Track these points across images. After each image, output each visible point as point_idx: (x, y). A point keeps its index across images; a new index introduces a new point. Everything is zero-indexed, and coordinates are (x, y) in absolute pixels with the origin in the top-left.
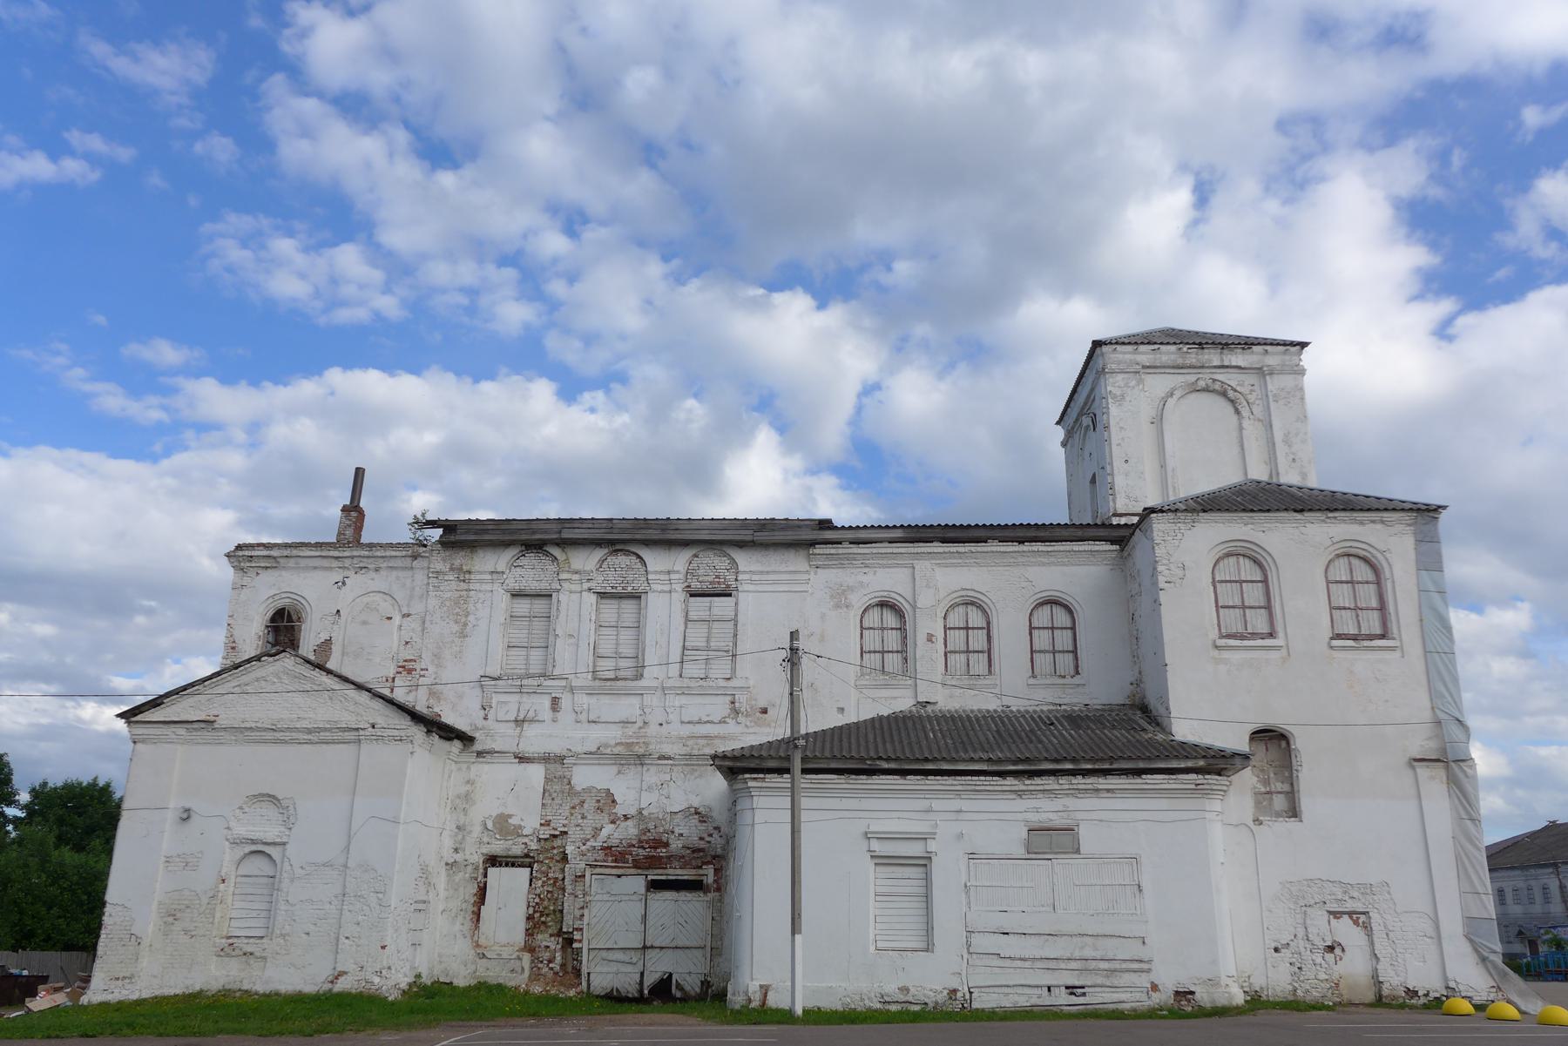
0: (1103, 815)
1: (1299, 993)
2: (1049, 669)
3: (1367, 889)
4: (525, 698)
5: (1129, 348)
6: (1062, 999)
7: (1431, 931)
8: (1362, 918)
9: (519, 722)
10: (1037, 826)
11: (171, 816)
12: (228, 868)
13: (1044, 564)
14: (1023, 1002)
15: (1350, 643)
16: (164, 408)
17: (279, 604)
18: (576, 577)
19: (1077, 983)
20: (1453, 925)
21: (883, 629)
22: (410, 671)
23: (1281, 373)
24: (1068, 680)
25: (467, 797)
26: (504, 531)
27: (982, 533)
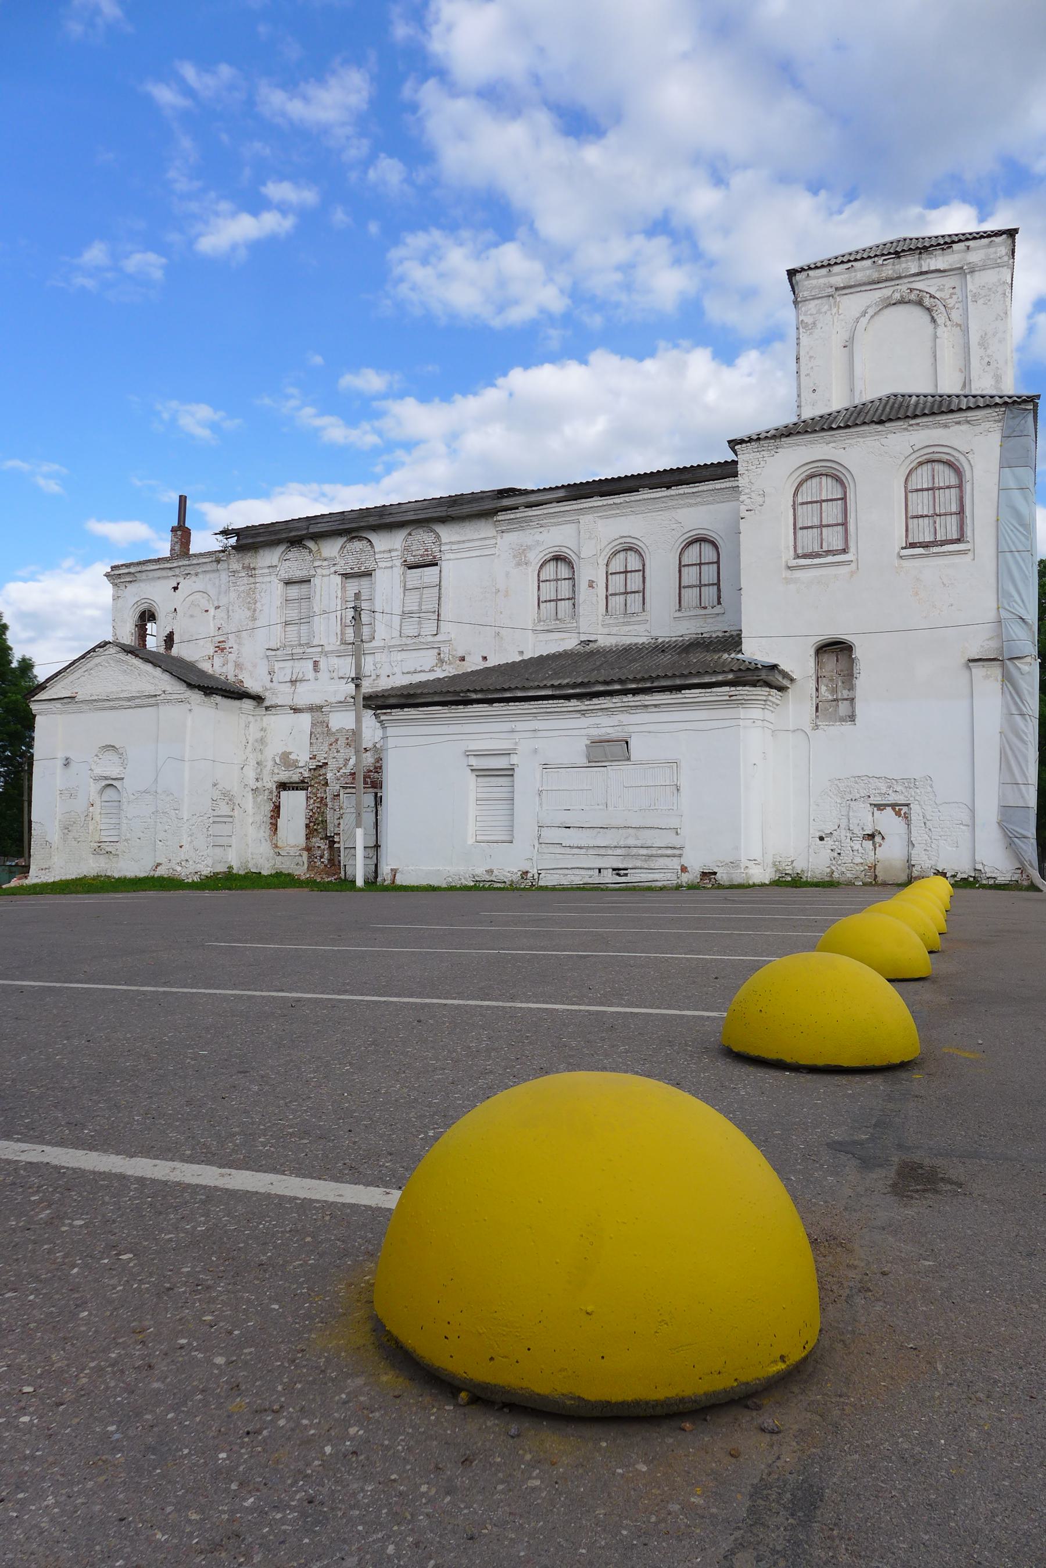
0: (651, 727)
1: (836, 875)
2: (695, 602)
3: (911, 783)
4: (297, 664)
5: (824, 271)
6: (609, 877)
7: (967, 819)
8: (905, 809)
9: (293, 682)
10: (597, 739)
11: (60, 763)
12: (94, 796)
13: (691, 505)
14: (577, 880)
15: (921, 551)
16: (380, 433)
17: (142, 608)
18: (325, 563)
19: (621, 866)
20: (988, 812)
21: (557, 580)
22: (222, 650)
23: (984, 268)
24: (709, 611)
25: (262, 741)
26: (271, 533)
27: (632, 484)
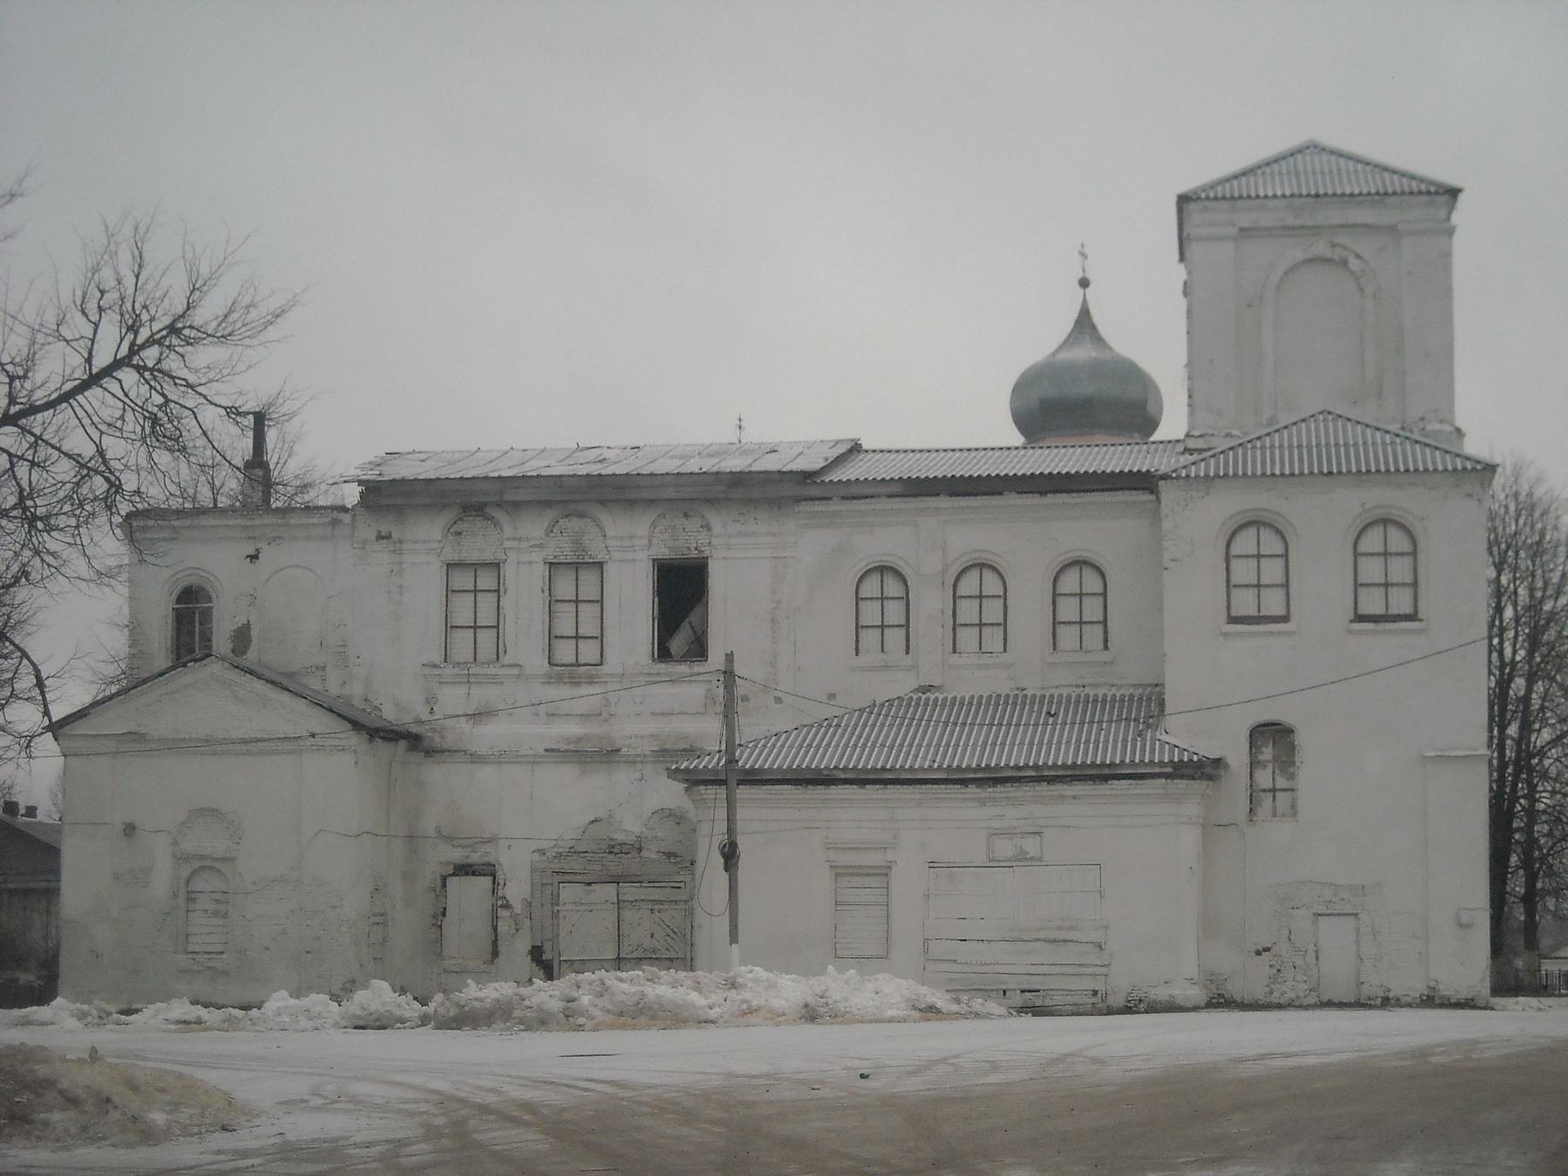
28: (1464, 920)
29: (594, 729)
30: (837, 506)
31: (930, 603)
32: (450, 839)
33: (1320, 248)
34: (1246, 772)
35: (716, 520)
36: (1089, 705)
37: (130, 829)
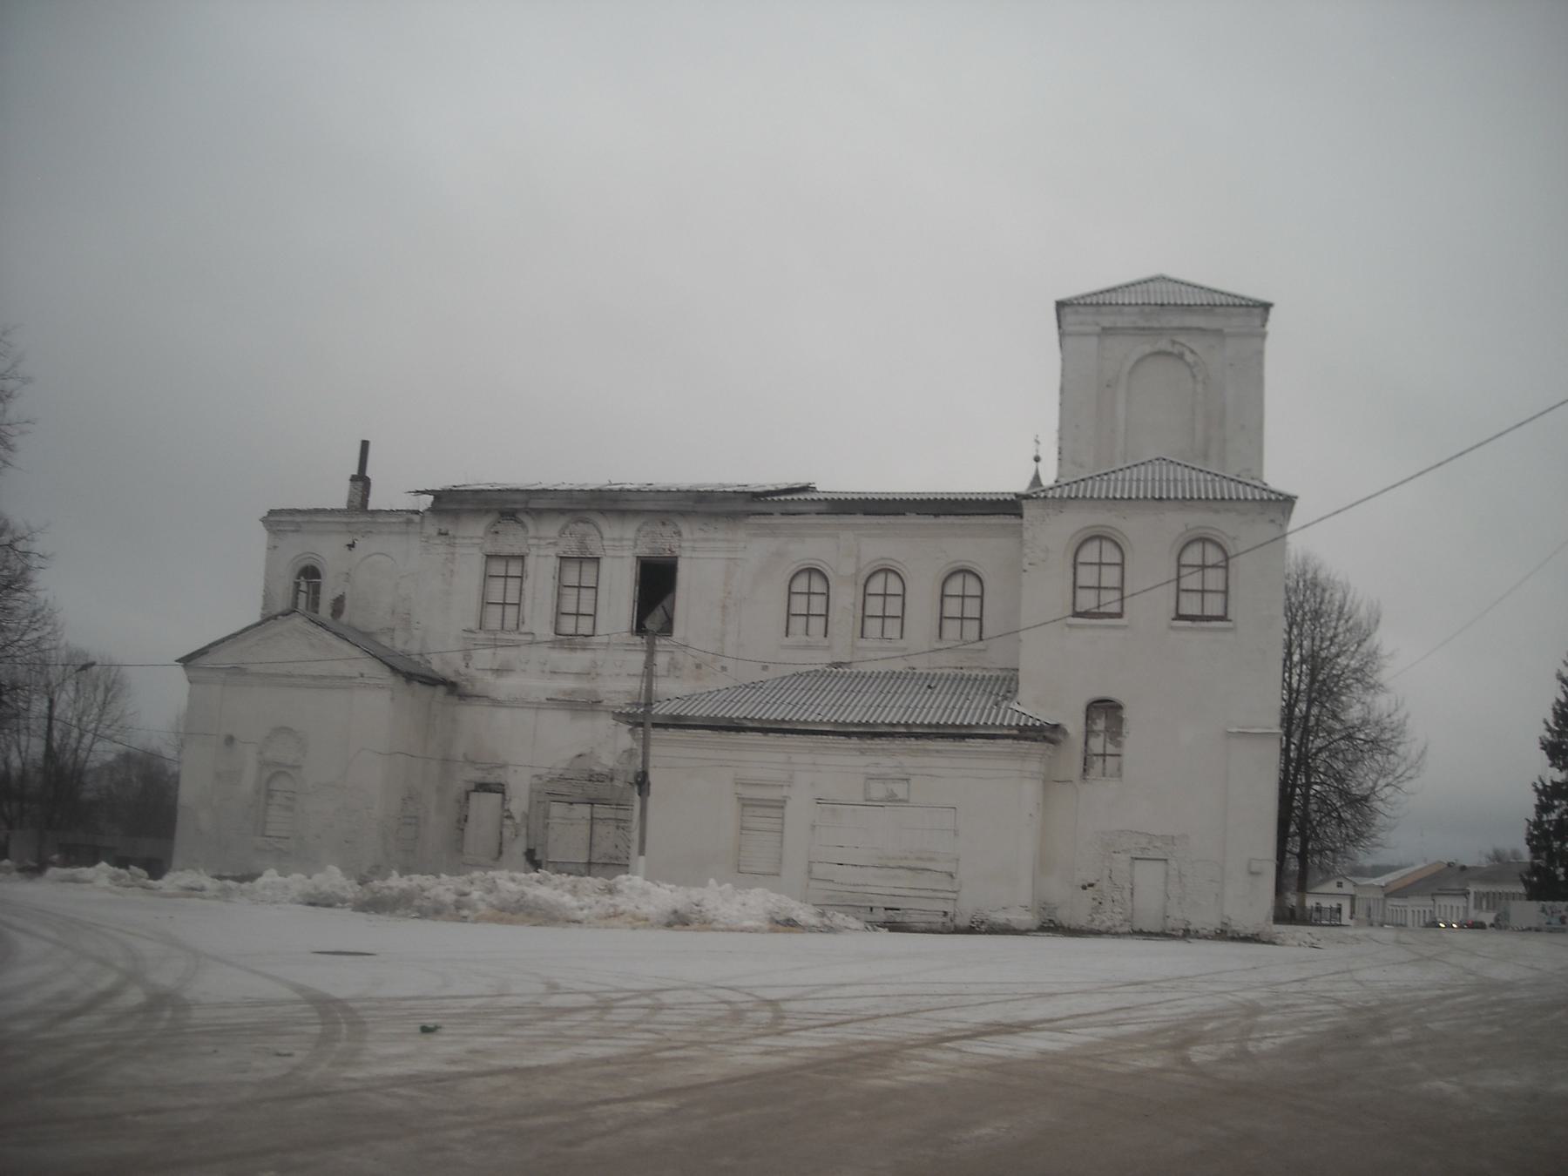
15: (1188, 623)
28: (1254, 869)
29: (585, 685)
30: (777, 520)
31: (845, 598)
32: (473, 763)
33: (1163, 344)
34: (1082, 740)
35: (685, 527)
36: (961, 681)
37: (230, 740)
